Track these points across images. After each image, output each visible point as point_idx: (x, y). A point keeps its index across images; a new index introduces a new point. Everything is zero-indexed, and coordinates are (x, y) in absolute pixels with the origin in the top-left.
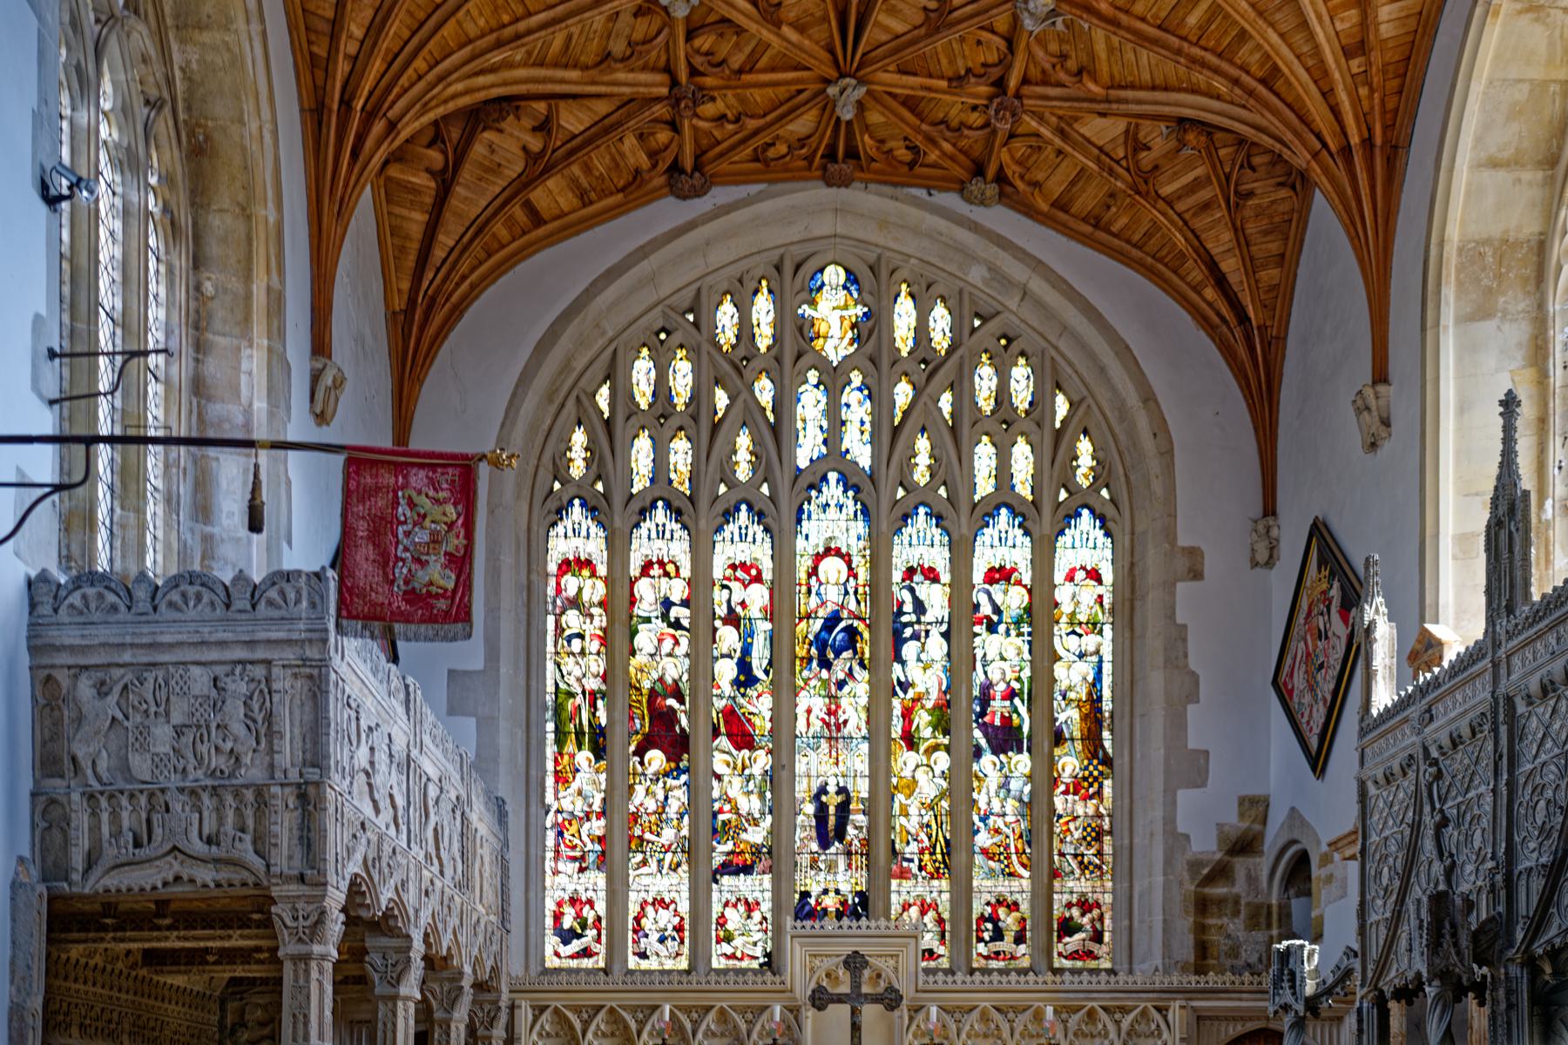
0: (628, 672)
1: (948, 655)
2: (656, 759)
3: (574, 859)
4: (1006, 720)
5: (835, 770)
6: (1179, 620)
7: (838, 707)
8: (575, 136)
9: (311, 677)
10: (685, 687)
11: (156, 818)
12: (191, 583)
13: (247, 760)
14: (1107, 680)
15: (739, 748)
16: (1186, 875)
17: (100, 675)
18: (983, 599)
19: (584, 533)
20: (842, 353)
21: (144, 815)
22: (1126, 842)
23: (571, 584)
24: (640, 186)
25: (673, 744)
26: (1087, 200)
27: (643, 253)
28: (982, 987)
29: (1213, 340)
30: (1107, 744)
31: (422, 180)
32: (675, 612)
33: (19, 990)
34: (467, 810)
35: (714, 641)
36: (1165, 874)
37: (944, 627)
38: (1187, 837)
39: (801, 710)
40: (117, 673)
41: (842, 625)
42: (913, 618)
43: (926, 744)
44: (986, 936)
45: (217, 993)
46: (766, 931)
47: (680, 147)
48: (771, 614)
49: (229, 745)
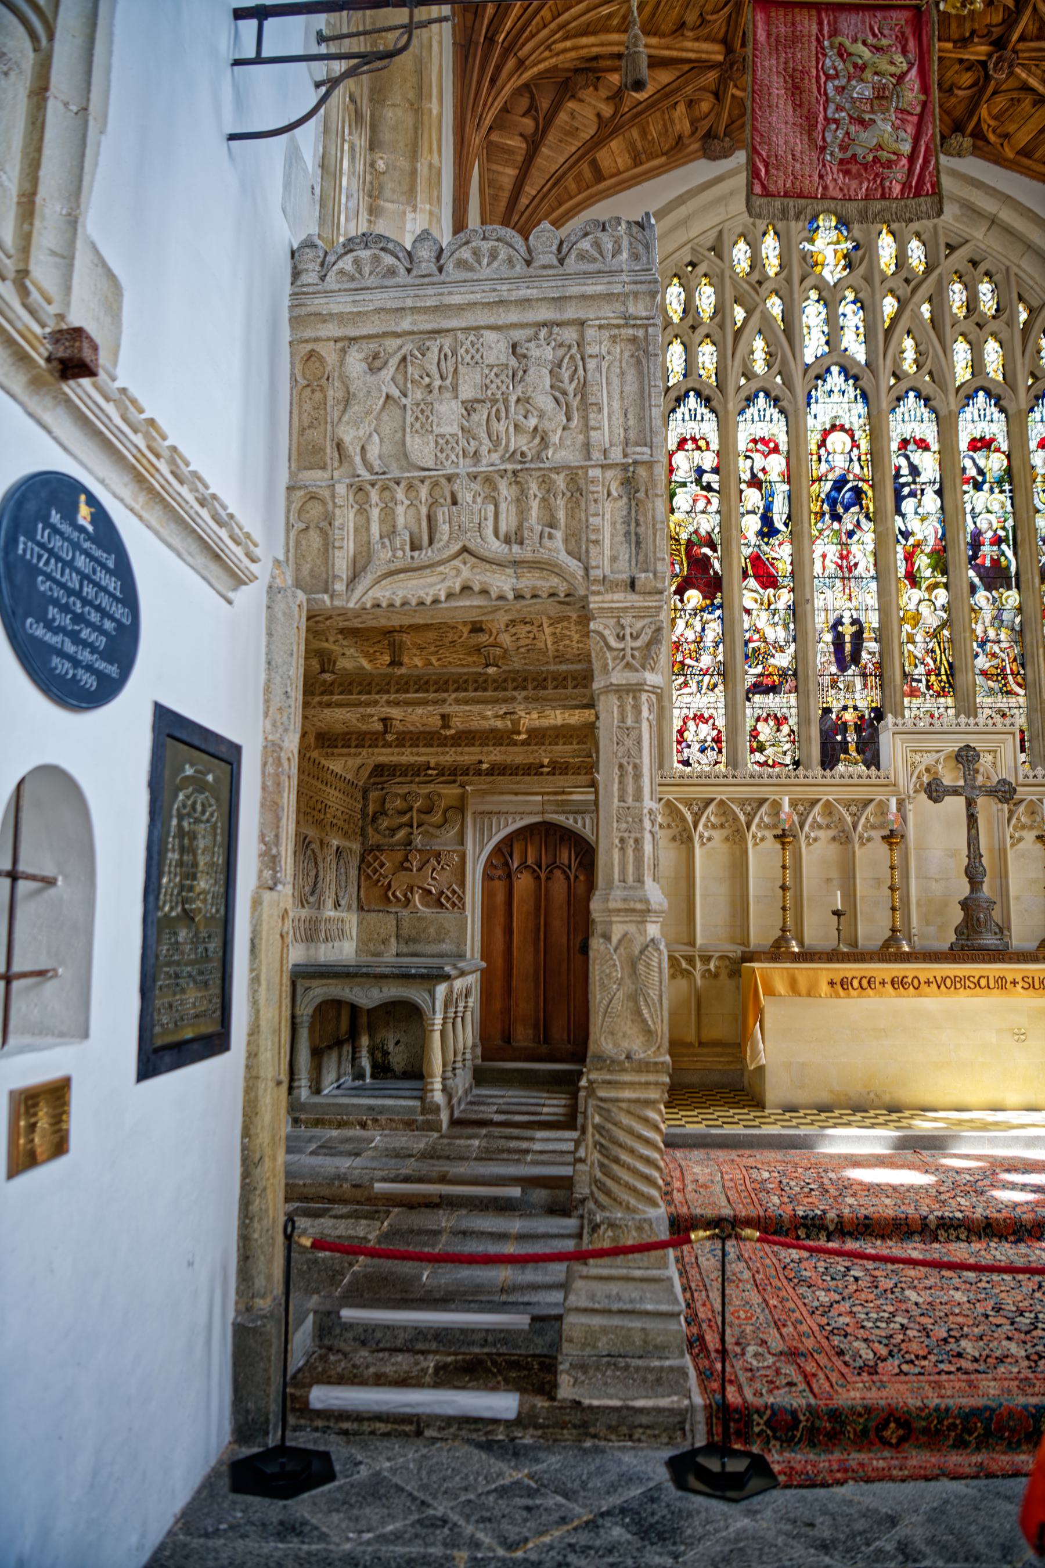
1: (942, 508)
2: (694, 597)
4: (996, 562)
5: (849, 605)
7: (849, 552)
9: (634, 340)
10: (716, 538)
11: (442, 514)
12: (484, 238)
13: (555, 438)
15: (765, 587)
17: (373, 346)
20: (837, 276)
21: (424, 510)
24: (680, 151)
25: (708, 584)
31: (516, 143)
32: (706, 478)
33: (274, 725)
37: (937, 486)
39: (817, 555)
40: (392, 344)
41: (849, 485)
42: (910, 479)
43: (928, 583)
45: (361, 784)
46: (793, 742)
48: (788, 477)
49: (533, 422)
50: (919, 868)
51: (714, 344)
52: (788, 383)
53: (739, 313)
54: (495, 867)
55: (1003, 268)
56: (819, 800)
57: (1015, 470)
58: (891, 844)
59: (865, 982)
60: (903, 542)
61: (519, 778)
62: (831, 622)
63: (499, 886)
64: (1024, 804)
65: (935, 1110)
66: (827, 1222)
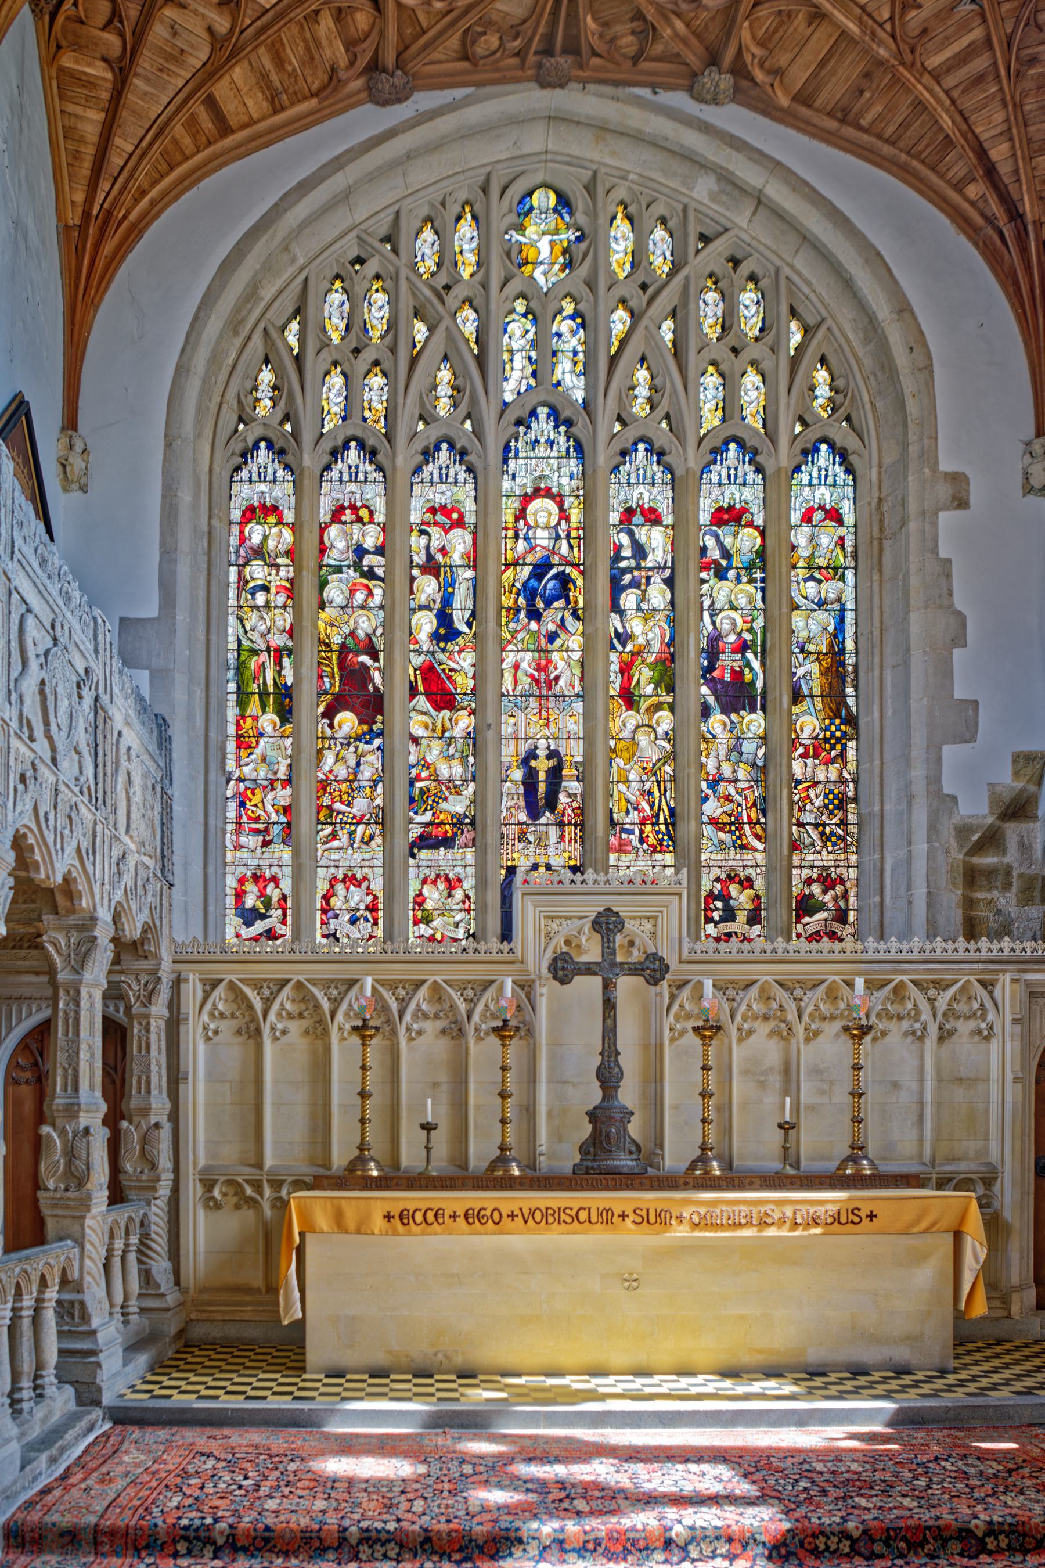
0: (316, 627)
1: (672, 603)
2: (347, 721)
3: (257, 831)
4: (737, 675)
6: (942, 554)
7: (549, 662)
8: (267, 11)
10: (379, 643)
14: (850, 631)
15: (438, 708)
16: (953, 842)
18: (710, 542)
19: (270, 477)
22: (877, 808)
23: (256, 533)
24: (335, 90)
25: (366, 704)
26: (832, 92)
27: (337, 164)
28: (763, 957)
29: (976, 244)
30: (851, 701)
31: (98, 71)
32: (368, 561)
34: (105, 699)
35: (412, 592)
36: (929, 841)
37: (667, 573)
38: (954, 799)
41: (554, 571)
43: (648, 703)
44: (716, 916)
46: (468, 911)
47: (382, 34)
48: (473, 561)
50: (552, 1068)
51: (385, 374)
52: (478, 433)
53: (420, 331)
54: (22, 1069)
55: (772, 270)
56: (424, 981)
57: (769, 550)
58: (503, 1038)
59: (430, 1216)
60: (619, 648)
61: (24, 952)
62: (522, 754)
63: (26, 1091)
64: (689, 986)
65: (519, 1375)
66: (216, 1535)
